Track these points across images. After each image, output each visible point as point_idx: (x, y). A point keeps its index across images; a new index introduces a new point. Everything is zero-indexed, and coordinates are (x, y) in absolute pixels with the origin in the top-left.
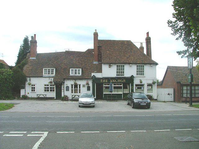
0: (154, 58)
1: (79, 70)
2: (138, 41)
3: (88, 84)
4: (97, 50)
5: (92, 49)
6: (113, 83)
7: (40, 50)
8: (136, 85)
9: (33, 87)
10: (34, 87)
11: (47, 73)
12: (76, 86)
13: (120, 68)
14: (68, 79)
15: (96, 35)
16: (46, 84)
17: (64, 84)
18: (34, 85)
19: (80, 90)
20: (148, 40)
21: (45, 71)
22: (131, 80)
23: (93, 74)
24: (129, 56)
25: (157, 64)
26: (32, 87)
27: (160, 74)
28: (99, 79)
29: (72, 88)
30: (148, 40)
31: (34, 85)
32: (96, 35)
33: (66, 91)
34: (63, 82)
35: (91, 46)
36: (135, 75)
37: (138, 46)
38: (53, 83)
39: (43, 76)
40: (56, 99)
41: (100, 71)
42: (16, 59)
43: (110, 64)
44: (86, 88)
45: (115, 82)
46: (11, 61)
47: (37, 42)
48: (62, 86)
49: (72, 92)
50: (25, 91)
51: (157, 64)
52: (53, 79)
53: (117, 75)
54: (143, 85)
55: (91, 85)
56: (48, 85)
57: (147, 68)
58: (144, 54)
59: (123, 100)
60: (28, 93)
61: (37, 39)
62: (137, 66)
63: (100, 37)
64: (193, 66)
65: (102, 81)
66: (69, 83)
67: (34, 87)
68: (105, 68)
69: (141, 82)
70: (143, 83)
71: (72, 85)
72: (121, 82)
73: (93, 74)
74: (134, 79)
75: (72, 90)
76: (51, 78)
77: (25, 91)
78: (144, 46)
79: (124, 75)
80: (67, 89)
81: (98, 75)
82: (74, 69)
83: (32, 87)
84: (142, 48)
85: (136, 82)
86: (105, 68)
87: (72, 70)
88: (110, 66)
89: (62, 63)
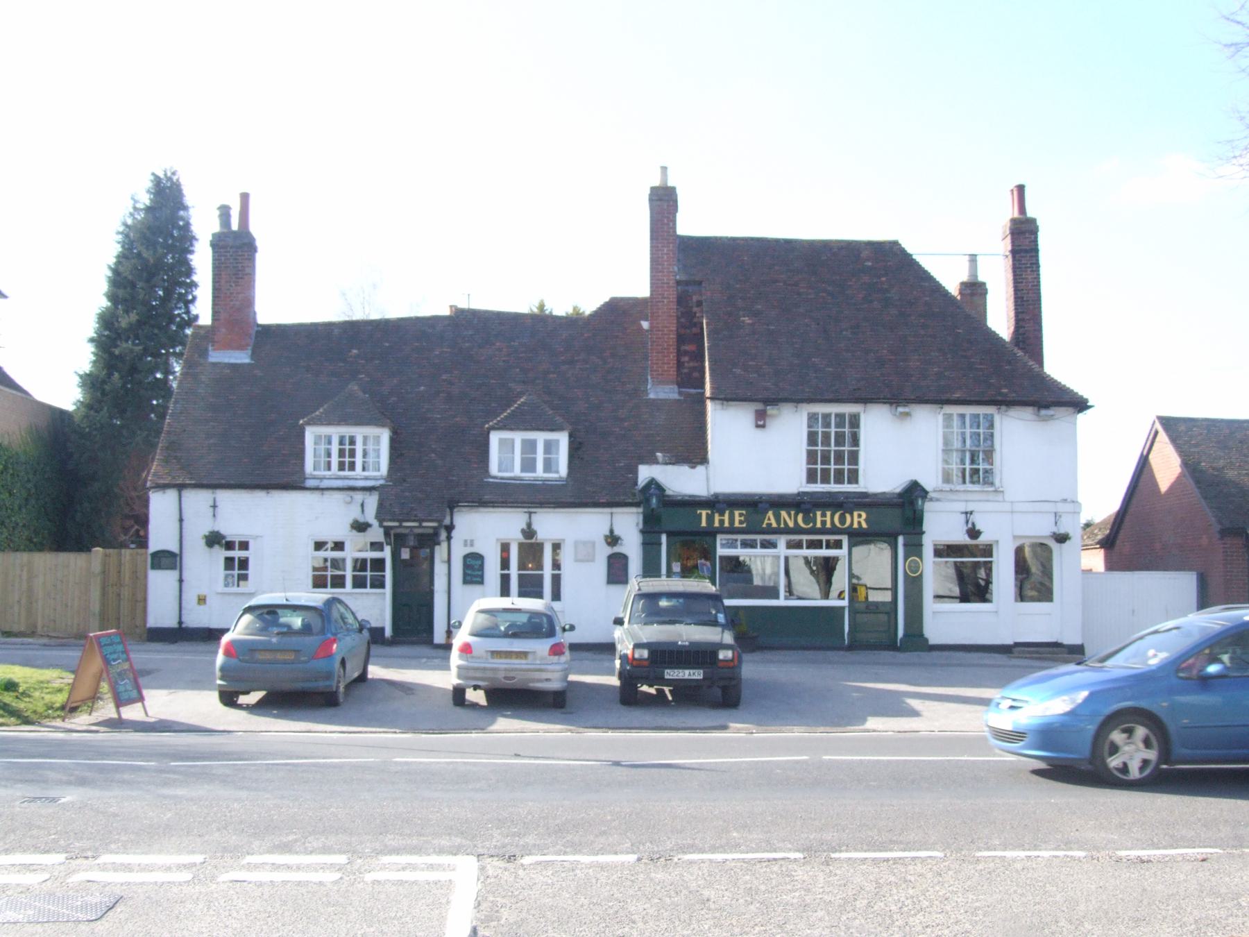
0: (1060, 362)
1: (550, 447)
2: (955, 248)
3: (613, 539)
4: (669, 306)
5: (642, 463)
6: (787, 531)
7: (280, 300)
8: (945, 551)
9: (237, 554)
10: (243, 554)
11: (335, 465)
12: (531, 550)
13: (833, 430)
14: (482, 503)
15: (664, 202)
16: (321, 539)
17: (449, 538)
18: (244, 546)
19: (556, 580)
20: (1024, 237)
21: (347, 460)
22: (901, 514)
23: (645, 473)
24: (285, 903)
25: (1080, 405)
26: (230, 554)
27: (1097, 465)
28: (693, 503)
29: (505, 564)
30: (1024, 237)
31: (244, 546)
32: (664, 202)
33: (1021, 597)
34: (447, 521)
35: (636, 283)
36: (930, 481)
37: (951, 279)
38: (376, 534)
39: (310, 483)
40: (393, 642)
41: (693, 451)
42: (84, 358)
43: (765, 399)
44: (600, 568)
45: (798, 530)
46: (58, 374)
47: (258, 243)
48: (440, 552)
49: (505, 592)
50: (181, 581)
51: (1080, 405)
52: (372, 502)
53: (811, 477)
54: (988, 550)
55: (632, 546)
56: (339, 546)
57: (1016, 433)
58: (992, 337)
59: (851, 647)
60: (202, 600)
61: (254, 229)
62: (948, 417)
63: (692, 222)
64: (140, 704)
65: (710, 519)
66: (484, 530)
67: (243, 554)
68: (727, 427)
69: (974, 533)
70: (983, 539)
71: (505, 548)
72: (834, 530)
73: (645, 473)
74: (928, 506)
75: (505, 580)
76: (359, 497)
77: (181, 581)
78: (682, 538)
79: (854, 477)
80: (473, 570)
81: (682, 481)
82: (518, 437)
83: (230, 554)
84: (975, 290)
85: (942, 525)
86: (727, 427)
87: (507, 445)
88: (761, 420)
89: (438, 388)
